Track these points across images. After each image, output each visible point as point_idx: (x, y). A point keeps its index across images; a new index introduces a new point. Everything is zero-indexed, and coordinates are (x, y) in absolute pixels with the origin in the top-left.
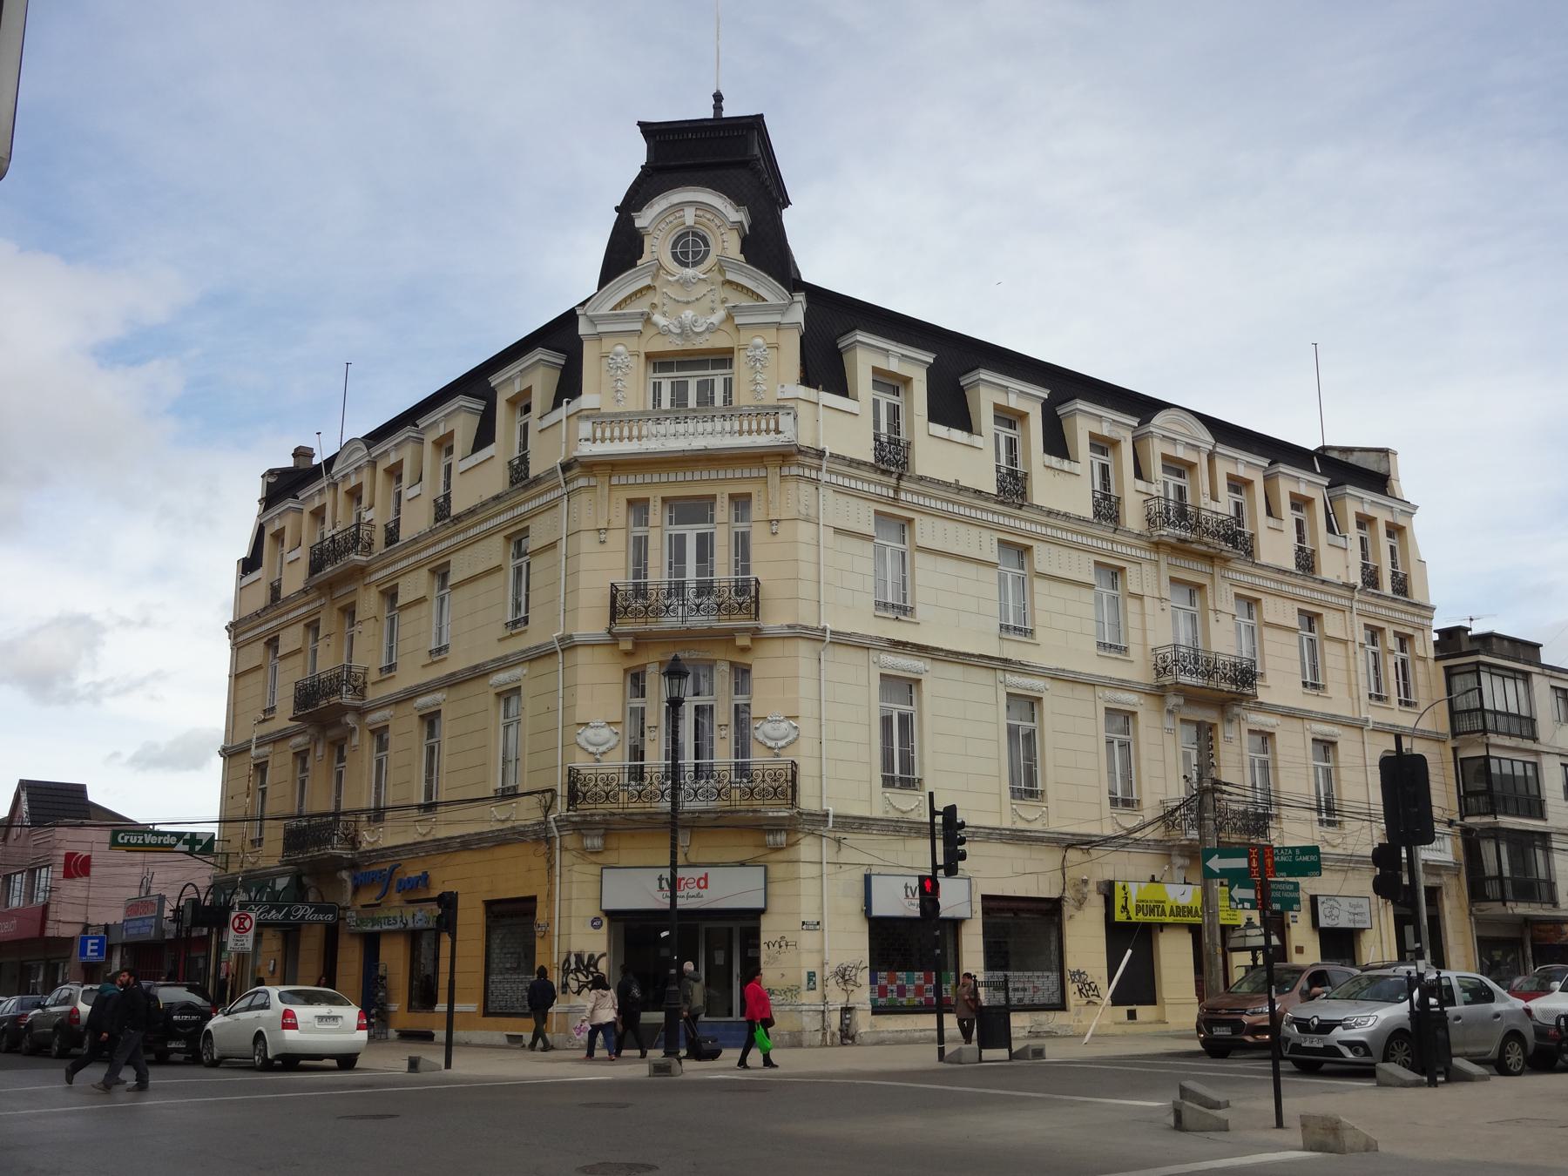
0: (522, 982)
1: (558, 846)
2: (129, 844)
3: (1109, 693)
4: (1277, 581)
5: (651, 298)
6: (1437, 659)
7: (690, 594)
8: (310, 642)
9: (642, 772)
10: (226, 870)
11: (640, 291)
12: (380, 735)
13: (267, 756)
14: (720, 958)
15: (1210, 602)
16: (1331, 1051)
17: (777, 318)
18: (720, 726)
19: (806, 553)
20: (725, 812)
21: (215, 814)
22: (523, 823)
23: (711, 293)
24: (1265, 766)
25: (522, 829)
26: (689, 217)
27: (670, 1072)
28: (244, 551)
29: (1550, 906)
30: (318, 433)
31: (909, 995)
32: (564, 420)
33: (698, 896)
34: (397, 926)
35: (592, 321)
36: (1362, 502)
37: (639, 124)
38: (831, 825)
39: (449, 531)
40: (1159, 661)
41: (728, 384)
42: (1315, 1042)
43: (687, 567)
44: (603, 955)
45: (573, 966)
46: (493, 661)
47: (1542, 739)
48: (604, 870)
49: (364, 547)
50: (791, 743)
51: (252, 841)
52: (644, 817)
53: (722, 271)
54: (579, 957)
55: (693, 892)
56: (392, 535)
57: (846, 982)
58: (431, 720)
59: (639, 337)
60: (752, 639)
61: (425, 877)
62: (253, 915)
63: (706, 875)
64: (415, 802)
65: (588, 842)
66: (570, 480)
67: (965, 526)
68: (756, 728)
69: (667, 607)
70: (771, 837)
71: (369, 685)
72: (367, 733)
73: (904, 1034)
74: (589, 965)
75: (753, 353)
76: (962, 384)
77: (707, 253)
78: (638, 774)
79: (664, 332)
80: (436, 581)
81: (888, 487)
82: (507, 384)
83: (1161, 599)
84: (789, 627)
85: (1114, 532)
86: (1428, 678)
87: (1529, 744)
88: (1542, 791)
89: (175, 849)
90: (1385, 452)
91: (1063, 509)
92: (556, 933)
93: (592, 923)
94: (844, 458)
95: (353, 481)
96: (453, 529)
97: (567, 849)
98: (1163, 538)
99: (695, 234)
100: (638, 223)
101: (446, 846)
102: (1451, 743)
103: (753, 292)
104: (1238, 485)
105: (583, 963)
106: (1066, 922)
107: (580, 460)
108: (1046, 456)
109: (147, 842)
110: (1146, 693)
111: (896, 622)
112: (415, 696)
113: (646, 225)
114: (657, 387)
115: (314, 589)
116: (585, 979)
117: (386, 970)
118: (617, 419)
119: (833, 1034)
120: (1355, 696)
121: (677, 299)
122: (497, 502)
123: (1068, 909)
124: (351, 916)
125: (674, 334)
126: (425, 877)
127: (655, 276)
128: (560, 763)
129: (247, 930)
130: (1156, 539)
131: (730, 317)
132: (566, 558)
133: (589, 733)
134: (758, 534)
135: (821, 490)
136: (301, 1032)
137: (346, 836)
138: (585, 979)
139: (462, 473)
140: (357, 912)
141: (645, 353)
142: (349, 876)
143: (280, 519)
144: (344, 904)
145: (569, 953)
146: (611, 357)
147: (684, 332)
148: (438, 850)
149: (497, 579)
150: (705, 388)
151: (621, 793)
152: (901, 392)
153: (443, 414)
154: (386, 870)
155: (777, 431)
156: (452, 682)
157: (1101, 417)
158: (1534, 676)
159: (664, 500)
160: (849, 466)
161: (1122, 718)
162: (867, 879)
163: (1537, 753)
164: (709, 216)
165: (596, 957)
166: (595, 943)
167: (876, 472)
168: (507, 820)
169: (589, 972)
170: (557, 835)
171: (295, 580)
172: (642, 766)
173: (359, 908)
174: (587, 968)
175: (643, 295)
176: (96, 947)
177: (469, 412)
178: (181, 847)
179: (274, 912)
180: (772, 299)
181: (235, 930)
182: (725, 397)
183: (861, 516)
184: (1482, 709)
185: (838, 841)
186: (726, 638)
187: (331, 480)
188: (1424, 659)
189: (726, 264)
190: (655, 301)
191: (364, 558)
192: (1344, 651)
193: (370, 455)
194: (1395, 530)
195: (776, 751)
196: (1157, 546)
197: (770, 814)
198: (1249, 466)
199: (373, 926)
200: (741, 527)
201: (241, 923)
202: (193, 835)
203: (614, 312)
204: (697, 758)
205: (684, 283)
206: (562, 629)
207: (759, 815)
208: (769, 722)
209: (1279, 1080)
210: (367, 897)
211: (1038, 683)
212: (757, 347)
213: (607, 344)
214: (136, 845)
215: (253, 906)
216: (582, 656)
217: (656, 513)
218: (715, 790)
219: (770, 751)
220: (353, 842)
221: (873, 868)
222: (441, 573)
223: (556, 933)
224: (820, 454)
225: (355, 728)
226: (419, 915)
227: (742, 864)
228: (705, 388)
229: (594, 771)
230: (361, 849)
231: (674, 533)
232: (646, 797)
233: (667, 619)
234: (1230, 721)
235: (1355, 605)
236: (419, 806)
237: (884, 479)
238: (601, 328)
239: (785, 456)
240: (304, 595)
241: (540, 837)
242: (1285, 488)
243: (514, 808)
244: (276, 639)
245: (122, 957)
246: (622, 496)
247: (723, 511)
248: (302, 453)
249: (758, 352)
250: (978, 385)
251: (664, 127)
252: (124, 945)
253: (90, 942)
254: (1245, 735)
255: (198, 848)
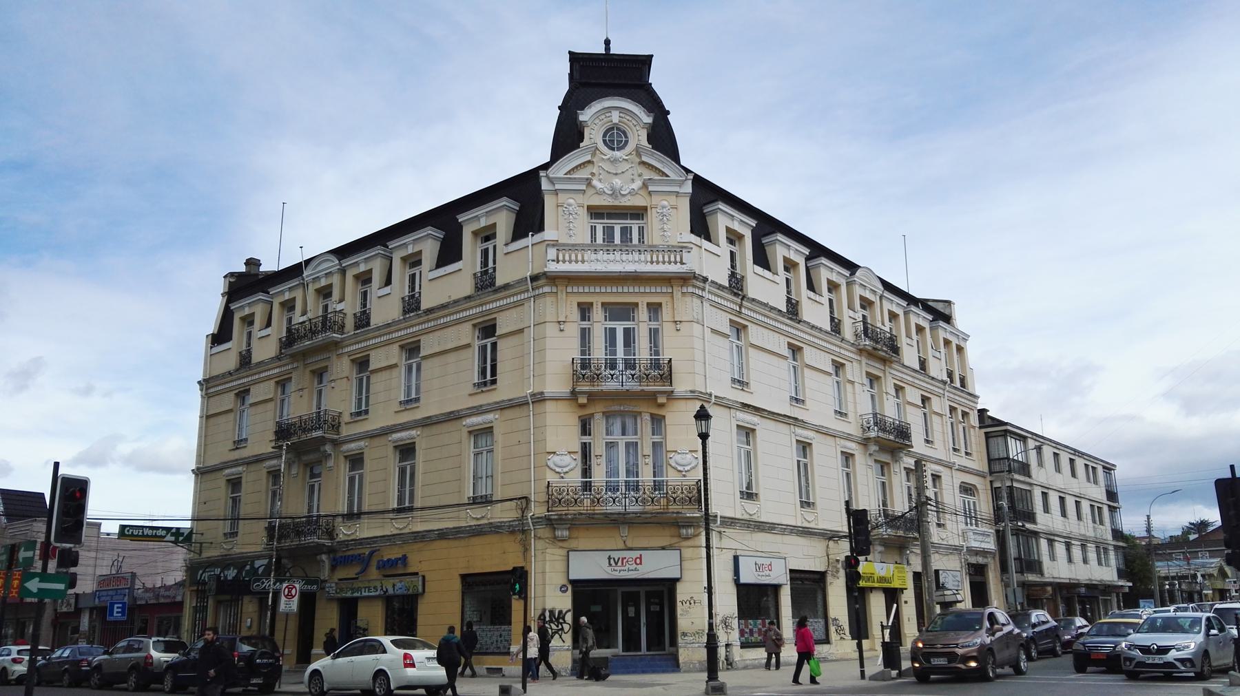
0: (490, 631)
1: (533, 535)
2: (132, 535)
3: (843, 442)
4: (912, 377)
5: (589, 169)
6: (980, 428)
7: (621, 366)
8: (279, 394)
9: (638, 486)
10: (200, 554)
11: (584, 164)
12: (356, 461)
13: (241, 474)
14: (631, 612)
15: (884, 388)
16: (1169, 665)
17: (676, 189)
18: (596, 456)
19: (698, 344)
20: (658, 513)
21: (189, 514)
22: (499, 520)
23: (632, 169)
24: (234, 499)
25: (499, 524)
26: (615, 117)
27: (723, 691)
28: (211, 327)
29: (1040, 576)
30: (301, 247)
31: (756, 635)
32: (530, 246)
33: (636, 569)
34: (377, 593)
35: (551, 181)
36: (946, 332)
37: (570, 52)
38: (719, 522)
39: (421, 319)
40: (865, 423)
41: (641, 230)
42: (1158, 659)
43: (618, 351)
44: (569, 611)
45: (548, 619)
46: (467, 409)
47: (1033, 477)
48: (570, 553)
49: (339, 328)
50: (693, 468)
51: (225, 534)
52: (601, 516)
53: (639, 155)
54: (552, 612)
55: (631, 567)
56: (363, 320)
57: (727, 627)
58: (407, 451)
59: (583, 194)
60: (667, 399)
61: (404, 558)
62: (297, 586)
63: (641, 555)
64: (391, 507)
65: (559, 533)
66: (537, 287)
67: (772, 332)
68: (670, 458)
69: (584, 376)
70: (684, 531)
71: (343, 424)
72: (342, 459)
73: (757, 661)
74: (559, 618)
75: (661, 211)
76: (763, 242)
77: (626, 142)
78: (587, 487)
79: (600, 193)
80: (404, 354)
81: (736, 304)
82: (471, 222)
83: (862, 384)
84: (691, 392)
85: (841, 342)
86: (977, 438)
87: (1027, 479)
88: (1034, 505)
89: (165, 539)
90: (948, 303)
91: (819, 326)
92: (533, 596)
93: (561, 588)
94: (716, 283)
95: (323, 282)
96: (426, 318)
97: (540, 538)
98: (867, 347)
99: (618, 129)
100: (581, 118)
101: (423, 537)
102: (989, 478)
103: (660, 170)
104: (893, 316)
105: (555, 617)
106: (829, 587)
107: (548, 274)
108: (808, 291)
109: (145, 534)
110: (859, 443)
111: (741, 392)
112: (392, 432)
113: (587, 120)
114: (593, 229)
115: (288, 357)
116: (556, 628)
117: (367, 624)
118: (574, 247)
119: (723, 662)
120: (947, 449)
121: (609, 171)
122: (468, 300)
123: (829, 579)
124: (331, 588)
125: (608, 195)
126: (404, 558)
127: (594, 154)
128: (533, 479)
129: (293, 597)
130: (861, 347)
131: (645, 186)
132: (534, 340)
133: (556, 459)
134: (667, 331)
135: (704, 303)
136: (419, 669)
137: (327, 530)
138: (556, 628)
139: (430, 280)
140: (336, 583)
141: (588, 206)
142: (327, 559)
143: (250, 307)
144: (322, 578)
145: (544, 610)
146: (565, 206)
147: (615, 193)
148: (415, 539)
149: (464, 354)
150: (625, 232)
151: (585, 500)
152: (737, 243)
153: (413, 238)
154: (365, 554)
155: (682, 263)
156: (427, 423)
157: (832, 269)
158: (1029, 440)
159: (603, 304)
160: (718, 289)
161: (847, 457)
162: (736, 559)
163: (1031, 484)
164: (628, 118)
165: (564, 612)
166: (564, 602)
167: (731, 294)
168: (483, 517)
169: (559, 623)
170: (532, 529)
171: (265, 348)
172: (638, 482)
173: (337, 581)
174: (557, 620)
175: (584, 167)
176: (120, 610)
177: (435, 239)
178: (169, 538)
179: (278, 584)
180: (673, 176)
181: (286, 596)
182: (639, 239)
183: (722, 321)
184: (1008, 458)
185: (720, 532)
186: (652, 397)
187: (302, 281)
188: (974, 427)
189: (641, 150)
190: (594, 171)
191: (340, 336)
192: (941, 420)
193: (341, 265)
194: (960, 349)
195: (684, 473)
196: (861, 351)
197: (688, 515)
198: (897, 306)
199: (352, 593)
200: (654, 325)
201: (289, 592)
202: (178, 529)
203: (568, 176)
204: (654, 476)
205: (614, 161)
206: (532, 387)
207: (680, 515)
208: (558, 455)
209: (526, 680)
210: (342, 573)
211: (811, 434)
212: (664, 207)
213: (562, 198)
214: (137, 536)
215: (264, 580)
216: (550, 406)
217: (598, 314)
218: (634, 499)
219: (680, 473)
220: (331, 534)
221: (738, 551)
222: (412, 349)
223: (533, 596)
224: (705, 280)
225: (331, 454)
226: (399, 585)
227: (663, 548)
228: (625, 232)
229: (566, 485)
230: (338, 540)
231: (608, 326)
232: (603, 502)
233: (611, 384)
234: (896, 461)
235: (946, 394)
236: (393, 510)
237: (735, 298)
238: (557, 187)
239: (686, 279)
240: (277, 360)
241: (518, 530)
242: (914, 320)
243: (488, 510)
244: (247, 391)
245: (90, 617)
246: (575, 300)
247: (643, 314)
248: (252, 263)
249: (665, 210)
250: (775, 243)
251: (627, 58)
252: (92, 610)
253: (116, 606)
254: (902, 469)
255: (181, 538)
